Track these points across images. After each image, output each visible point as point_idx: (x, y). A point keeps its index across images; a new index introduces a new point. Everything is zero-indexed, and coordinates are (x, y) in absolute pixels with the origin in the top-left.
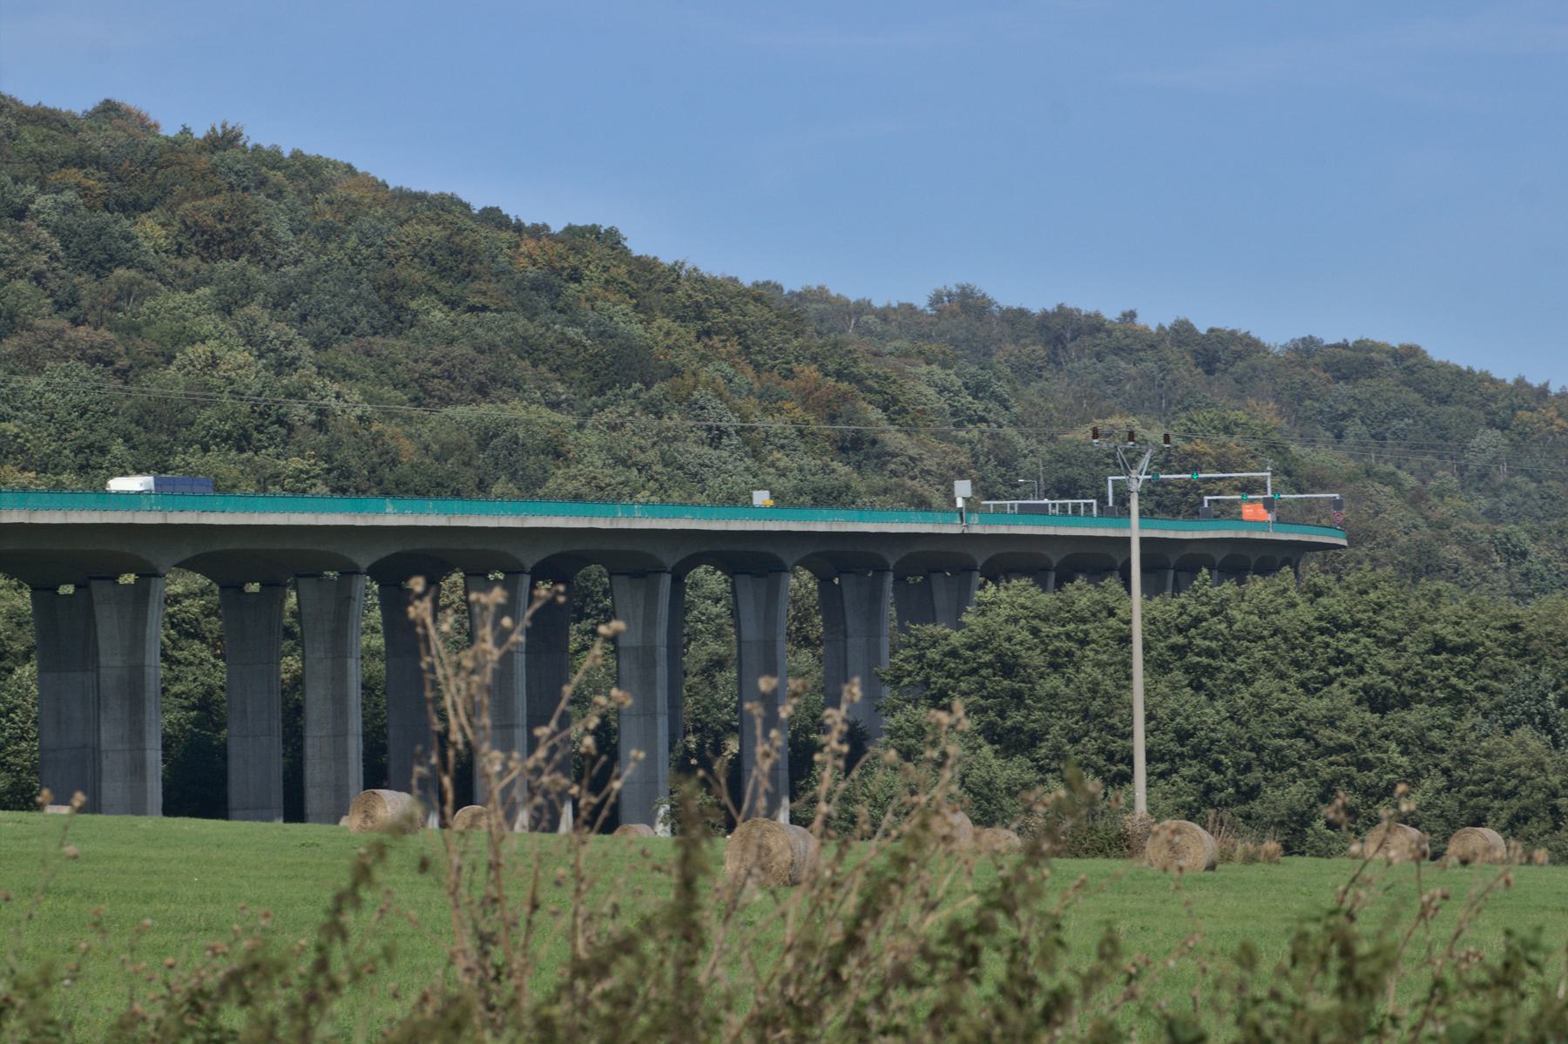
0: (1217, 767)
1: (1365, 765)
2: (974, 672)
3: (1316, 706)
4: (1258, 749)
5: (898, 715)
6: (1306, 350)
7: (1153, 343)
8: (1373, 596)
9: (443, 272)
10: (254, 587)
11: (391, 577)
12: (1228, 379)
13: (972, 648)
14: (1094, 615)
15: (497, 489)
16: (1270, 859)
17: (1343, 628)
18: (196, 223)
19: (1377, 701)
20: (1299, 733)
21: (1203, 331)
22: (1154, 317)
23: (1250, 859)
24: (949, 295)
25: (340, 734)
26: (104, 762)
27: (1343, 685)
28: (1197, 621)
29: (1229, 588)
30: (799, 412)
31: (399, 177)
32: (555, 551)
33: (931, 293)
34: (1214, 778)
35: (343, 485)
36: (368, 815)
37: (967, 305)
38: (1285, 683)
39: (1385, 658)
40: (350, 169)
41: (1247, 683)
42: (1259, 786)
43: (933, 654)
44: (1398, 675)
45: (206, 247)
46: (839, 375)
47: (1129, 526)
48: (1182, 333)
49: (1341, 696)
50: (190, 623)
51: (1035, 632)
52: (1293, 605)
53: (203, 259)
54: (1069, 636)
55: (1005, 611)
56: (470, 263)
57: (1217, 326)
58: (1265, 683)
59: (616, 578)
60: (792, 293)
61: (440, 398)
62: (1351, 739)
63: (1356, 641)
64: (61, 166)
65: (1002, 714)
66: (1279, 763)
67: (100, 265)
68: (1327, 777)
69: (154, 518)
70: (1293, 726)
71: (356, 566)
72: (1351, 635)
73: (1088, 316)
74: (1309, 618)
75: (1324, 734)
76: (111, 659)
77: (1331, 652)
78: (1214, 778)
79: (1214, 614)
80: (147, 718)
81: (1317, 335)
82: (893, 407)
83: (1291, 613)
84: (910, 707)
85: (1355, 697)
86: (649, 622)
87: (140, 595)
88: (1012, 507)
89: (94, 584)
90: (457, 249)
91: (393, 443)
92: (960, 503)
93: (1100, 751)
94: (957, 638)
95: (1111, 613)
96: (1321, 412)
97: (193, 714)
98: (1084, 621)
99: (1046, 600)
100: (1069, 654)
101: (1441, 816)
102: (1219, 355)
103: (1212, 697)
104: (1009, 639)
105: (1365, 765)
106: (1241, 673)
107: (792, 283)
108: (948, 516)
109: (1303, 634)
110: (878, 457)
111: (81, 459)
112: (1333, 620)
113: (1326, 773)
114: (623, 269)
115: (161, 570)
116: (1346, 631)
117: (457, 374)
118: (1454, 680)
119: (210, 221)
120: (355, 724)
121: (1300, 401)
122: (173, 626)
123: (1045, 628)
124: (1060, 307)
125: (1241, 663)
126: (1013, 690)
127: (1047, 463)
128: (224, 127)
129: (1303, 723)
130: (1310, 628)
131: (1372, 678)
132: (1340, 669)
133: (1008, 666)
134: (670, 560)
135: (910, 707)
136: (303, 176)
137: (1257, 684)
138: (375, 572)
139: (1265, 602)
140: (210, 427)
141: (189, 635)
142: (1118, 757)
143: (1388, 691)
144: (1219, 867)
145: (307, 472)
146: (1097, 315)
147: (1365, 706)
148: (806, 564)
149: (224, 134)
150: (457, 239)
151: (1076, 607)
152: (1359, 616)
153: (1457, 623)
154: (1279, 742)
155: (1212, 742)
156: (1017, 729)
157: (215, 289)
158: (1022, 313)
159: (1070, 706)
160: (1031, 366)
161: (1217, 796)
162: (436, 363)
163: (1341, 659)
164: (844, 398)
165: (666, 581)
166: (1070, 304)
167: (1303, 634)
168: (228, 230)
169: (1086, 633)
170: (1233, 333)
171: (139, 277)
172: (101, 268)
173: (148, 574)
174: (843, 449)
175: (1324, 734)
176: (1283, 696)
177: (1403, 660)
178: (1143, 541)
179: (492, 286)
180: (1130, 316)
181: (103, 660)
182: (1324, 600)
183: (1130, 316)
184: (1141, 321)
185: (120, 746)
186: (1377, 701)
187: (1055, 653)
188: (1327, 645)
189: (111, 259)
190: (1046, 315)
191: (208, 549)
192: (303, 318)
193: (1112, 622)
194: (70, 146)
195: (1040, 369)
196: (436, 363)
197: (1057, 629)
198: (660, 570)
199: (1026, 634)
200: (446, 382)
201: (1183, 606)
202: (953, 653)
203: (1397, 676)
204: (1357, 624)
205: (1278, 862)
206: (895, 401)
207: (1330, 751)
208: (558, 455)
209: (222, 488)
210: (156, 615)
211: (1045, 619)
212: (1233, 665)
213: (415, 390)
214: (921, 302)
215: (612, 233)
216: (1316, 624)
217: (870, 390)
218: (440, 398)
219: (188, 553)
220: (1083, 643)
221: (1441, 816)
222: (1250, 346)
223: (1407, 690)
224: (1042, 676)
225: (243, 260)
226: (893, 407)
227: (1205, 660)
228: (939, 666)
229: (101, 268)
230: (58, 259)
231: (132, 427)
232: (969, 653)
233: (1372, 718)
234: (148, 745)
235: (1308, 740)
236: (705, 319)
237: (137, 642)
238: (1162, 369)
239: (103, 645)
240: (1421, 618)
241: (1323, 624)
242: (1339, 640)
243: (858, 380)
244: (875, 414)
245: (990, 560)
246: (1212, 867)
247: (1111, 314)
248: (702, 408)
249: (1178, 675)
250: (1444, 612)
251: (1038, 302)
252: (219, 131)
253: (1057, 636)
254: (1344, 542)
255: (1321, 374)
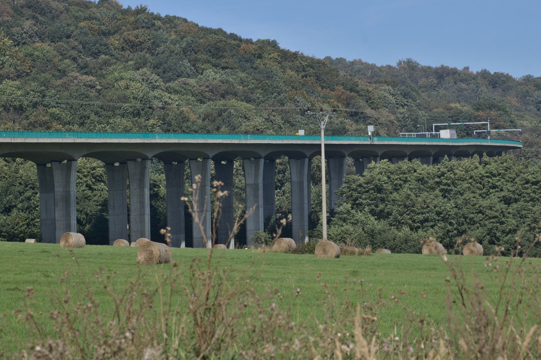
0: (451, 224)
1: (502, 223)
2: (367, 192)
3: (485, 203)
4: (466, 218)
5: (341, 207)
6: (528, 79)
7: (474, 77)
8: (505, 164)
9: (213, 56)
10: (117, 164)
11: (270, 160)
12: (500, 90)
13: (367, 183)
14: (409, 171)
15: (223, 129)
16: (368, 254)
17: (494, 176)
18: (128, 39)
19: (507, 201)
20: (480, 212)
21: (492, 73)
22: (474, 69)
23: (361, 254)
24: (404, 62)
25: (142, 214)
26: (57, 224)
27: (494, 195)
28: (443, 174)
29: (454, 162)
30: (335, 103)
31: (203, 23)
32: (161, 151)
33: (398, 61)
34: (450, 228)
35: (167, 130)
36: (67, 241)
37: (410, 66)
38: (475, 195)
39: (509, 186)
40: (185, 20)
41: (462, 194)
42: (466, 230)
43: (354, 186)
44: (514, 192)
45: (132, 47)
46: (351, 90)
47: (320, 139)
48: (484, 74)
49: (494, 198)
50: (99, 177)
51: (389, 177)
52: (477, 168)
53: (131, 52)
54: (400, 179)
55: (378, 170)
56: (223, 53)
57: (497, 71)
58: (468, 195)
59: (245, 161)
60: (349, 61)
61: (208, 99)
62: (497, 214)
63: (499, 180)
64: (84, 20)
65: (377, 206)
66: (473, 222)
67: (96, 54)
68: (490, 227)
69: (450, 144)
70: (477, 210)
71: (147, 157)
72: (498, 178)
73: (452, 69)
74: (483, 172)
75: (488, 212)
76: (59, 189)
77: (490, 185)
78: (450, 228)
79: (448, 171)
80: (71, 209)
81: (532, 74)
82: (369, 101)
83: (476, 171)
84: (345, 204)
85: (499, 199)
86: (256, 176)
87: (69, 168)
88: (414, 135)
89: (129, 162)
90: (220, 48)
91: (187, 114)
92: (370, 134)
93: (411, 219)
94: (362, 180)
95: (415, 171)
96: (532, 101)
97: (99, 207)
98: (405, 173)
99: (393, 167)
100: (400, 185)
101: (527, 240)
102: (498, 82)
103: (450, 200)
104: (379, 180)
105: (502, 223)
106: (459, 192)
107: (349, 58)
108: (365, 138)
109: (480, 178)
110: (364, 118)
111: (81, 121)
112: (491, 173)
113: (490, 226)
114: (276, 54)
115: (76, 158)
116: (496, 177)
117: (214, 90)
118: (531, 194)
119: (133, 38)
120: (148, 210)
121: (525, 97)
122: (93, 178)
123: (392, 176)
124: (442, 66)
125: (459, 188)
126: (381, 197)
127: (428, 120)
128: (141, 6)
129: (481, 208)
130: (483, 176)
131: (505, 193)
132: (494, 190)
133: (379, 190)
134: (308, 154)
135: (345, 204)
136: (168, 23)
137: (465, 195)
138: (213, 159)
139: (468, 167)
140: (127, 110)
141: (99, 181)
142: (416, 221)
143: (511, 197)
144: (341, 256)
145: (156, 125)
146: (455, 69)
147: (503, 202)
148: (350, 155)
149: (141, 8)
150: (218, 44)
151: (403, 169)
152: (500, 172)
153: (533, 174)
154: (472, 215)
155: (449, 215)
156: (382, 211)
157: (134, 62)
158: (429, 68)
159: (400, 203)
160: (432, 86)
161: (451, 234)
162: (207, 87)
163: (494, 187)
164: (352, 98)
165: (307, 160)
166: (445, 65)
167: (480, 178)
168: (139, 41)
169: (406, 178)
170: (502, 74)
171: (110, 58)
172: (96, 55)
173: (72, 160)
174: (351, 116)
175: (488, 212)
176: (475, 199)
177: (515, 187)
178: (325, 145)
179: (230, 60)
180: (467, 68)
181: (56, 189)
182: (487, 166)
183: (467, 68)
184: (470, 70)
185: (62, 219)
186: (507, 201)
187: (396, 185)
188: (489, 182)
189: (100, 52)
190: (437, 69)
191: (93, 151)
192: (164, 72)
193: (415, 174)
194: (87, 13)
195: (435, 87)
196: (207, 87)
197: (396, 177)
198: (306, 157)
199: (385, 178)
200: (210, 94)
201: (439, 169)
202: (360, 186)
203: (513, 192)
204: (499, 174)
205: (370, 255)
206: (370, 99)
207: (490, 218)
208: (246, 118)
209: (127, 131)
210: (74, 175)
211: (392, 174)
212: (456, 189)
213: (200, 97)
214: (394, 64)
215: (274, 42)
216: (485, 175)
217: (362, 95)
218: (208, 99)
219: (156, 152)
220: (406, 181)
221: (527, 240)
222: (508, 78)
223: (517, 197)
224: (391, 193)
225: (144, 52)
226: (369, 101)
227: (445, 187)
228: (355, 190)
229: (96, 55)
230: (81, 52)
231: (99, 110)
232: (366, 185)
233: (504, 206)
234: (72, 219)
235: (483, 214)
236: (306, 71)
237: (67, 182)
238: (477, 87)
239: (56, 184)
240: (521, 172)
241: (488, 174)
242: (493, 180)
243: (357, 92)
244: (362, 103)
245: (412, 153)
246: (338, 257)
247: (460, 68)
248: (298, 102)
249: (437, 192)
250: (529, 170)
251: (435, 64)
252: (140, 8)
253: (396, 179)
254: (521, 146)
255: (533, 88)
